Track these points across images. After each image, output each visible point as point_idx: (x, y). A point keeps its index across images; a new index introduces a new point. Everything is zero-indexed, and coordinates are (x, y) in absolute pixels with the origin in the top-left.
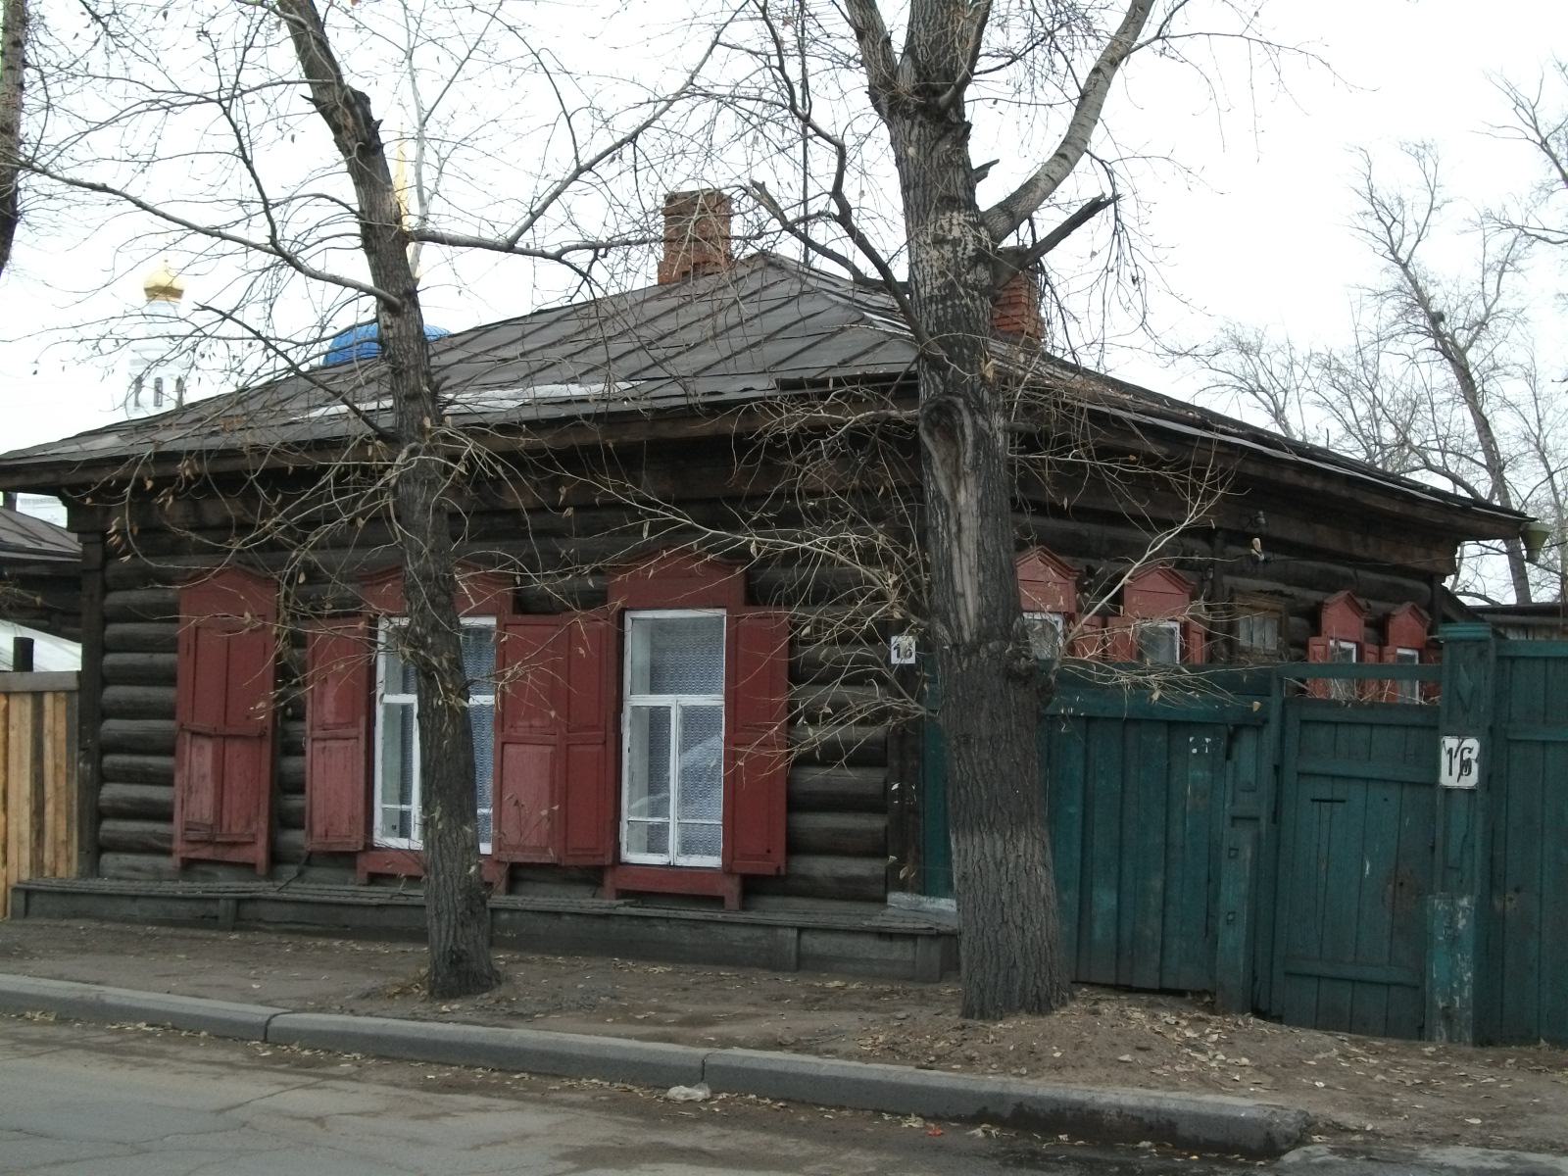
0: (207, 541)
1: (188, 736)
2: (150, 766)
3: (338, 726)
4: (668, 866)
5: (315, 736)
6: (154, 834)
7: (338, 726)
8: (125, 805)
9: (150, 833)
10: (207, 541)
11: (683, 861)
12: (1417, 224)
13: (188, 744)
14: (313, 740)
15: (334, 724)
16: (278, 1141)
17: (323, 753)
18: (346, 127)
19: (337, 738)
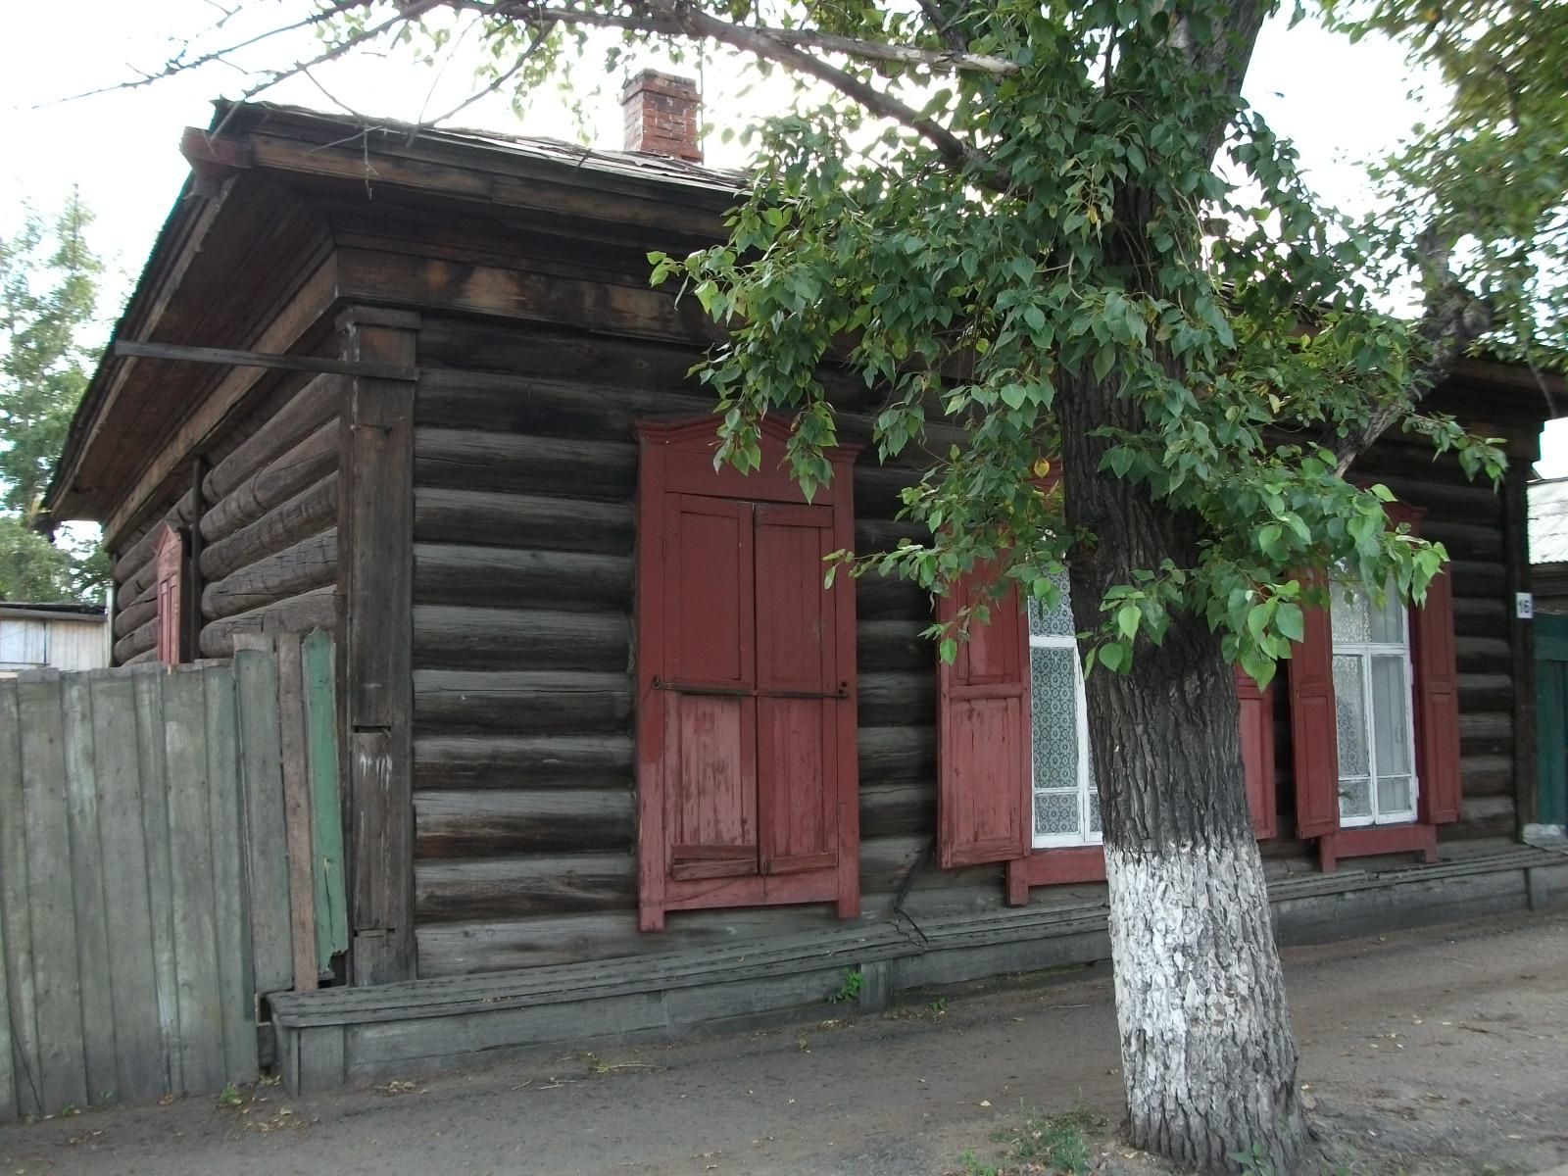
0: (95, 431)
1: (672, 698)
2: (550, 755)
3: (989, 679)
4: (1374, 824)
5: (954, 695)
6: (570, 879)
7: (989, 679)
8: (486, 831)
9: (557, 877)
10: (95, 431)
11: (1383, 819)
12: (182, 55)
13: (673, 713)
14: (951, 700)
15: (985, 676)
16: (1391, 413)
17: (970, 717)
18: (1381, 183)
19: (991, 697)
